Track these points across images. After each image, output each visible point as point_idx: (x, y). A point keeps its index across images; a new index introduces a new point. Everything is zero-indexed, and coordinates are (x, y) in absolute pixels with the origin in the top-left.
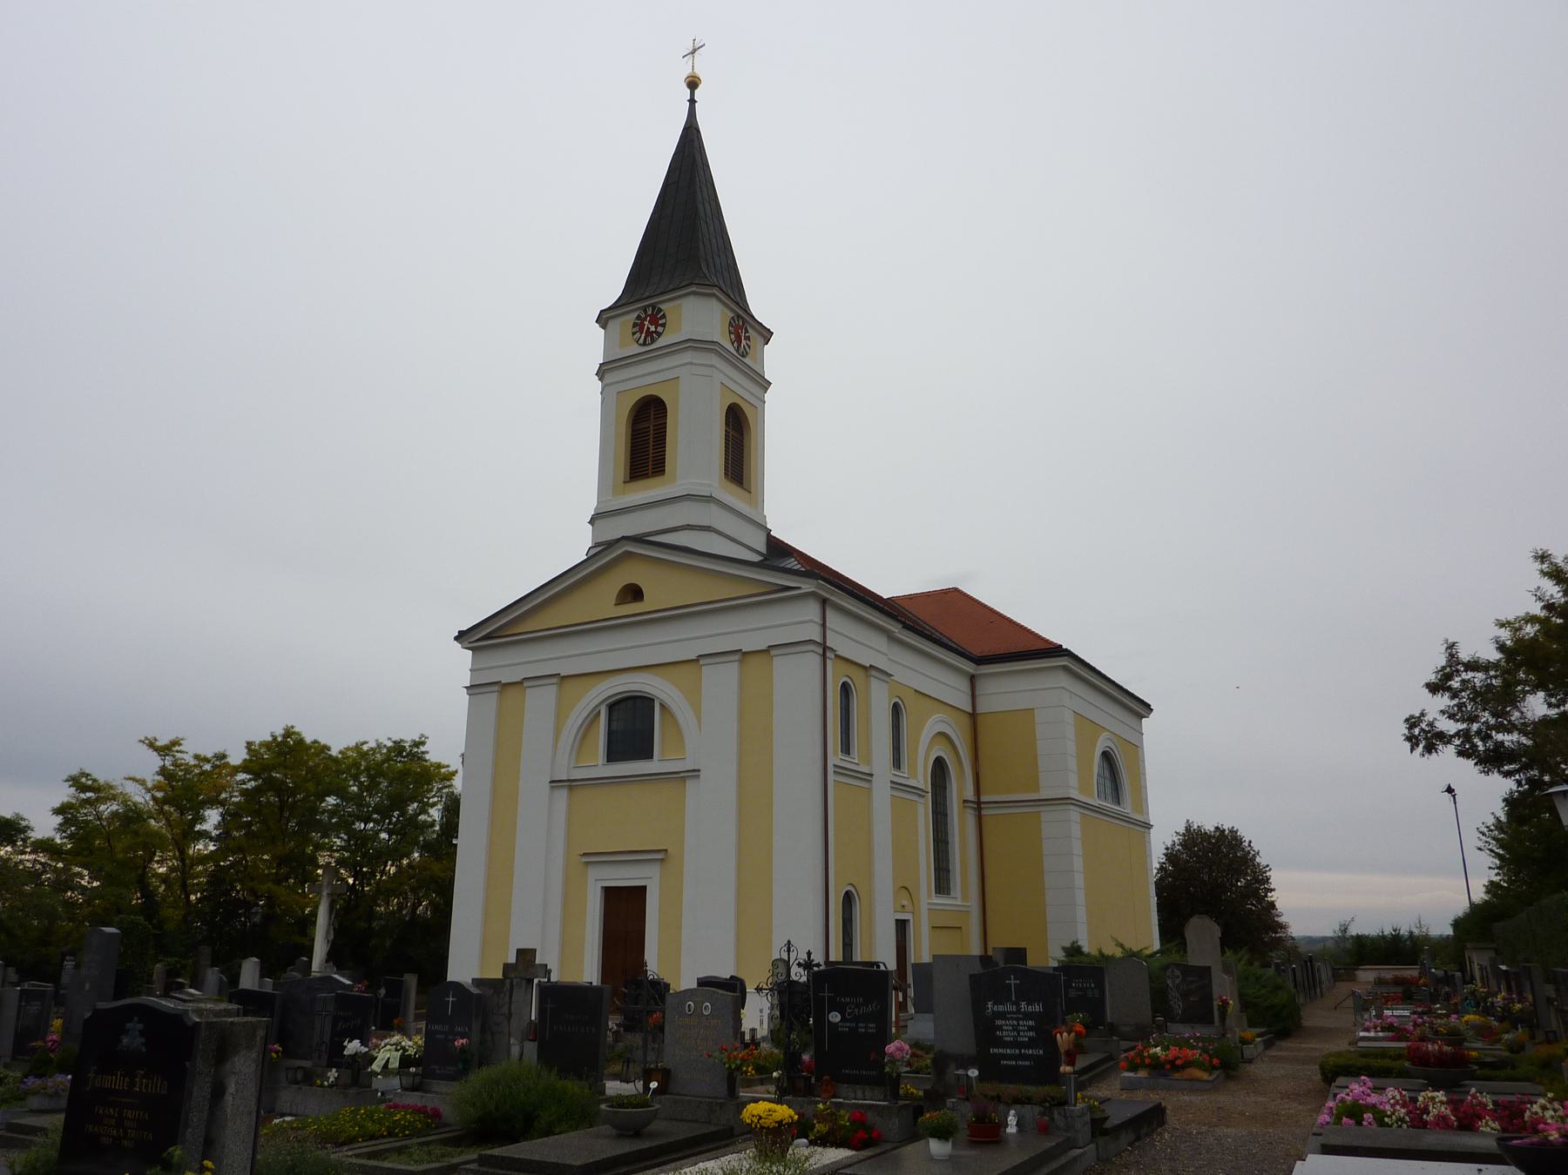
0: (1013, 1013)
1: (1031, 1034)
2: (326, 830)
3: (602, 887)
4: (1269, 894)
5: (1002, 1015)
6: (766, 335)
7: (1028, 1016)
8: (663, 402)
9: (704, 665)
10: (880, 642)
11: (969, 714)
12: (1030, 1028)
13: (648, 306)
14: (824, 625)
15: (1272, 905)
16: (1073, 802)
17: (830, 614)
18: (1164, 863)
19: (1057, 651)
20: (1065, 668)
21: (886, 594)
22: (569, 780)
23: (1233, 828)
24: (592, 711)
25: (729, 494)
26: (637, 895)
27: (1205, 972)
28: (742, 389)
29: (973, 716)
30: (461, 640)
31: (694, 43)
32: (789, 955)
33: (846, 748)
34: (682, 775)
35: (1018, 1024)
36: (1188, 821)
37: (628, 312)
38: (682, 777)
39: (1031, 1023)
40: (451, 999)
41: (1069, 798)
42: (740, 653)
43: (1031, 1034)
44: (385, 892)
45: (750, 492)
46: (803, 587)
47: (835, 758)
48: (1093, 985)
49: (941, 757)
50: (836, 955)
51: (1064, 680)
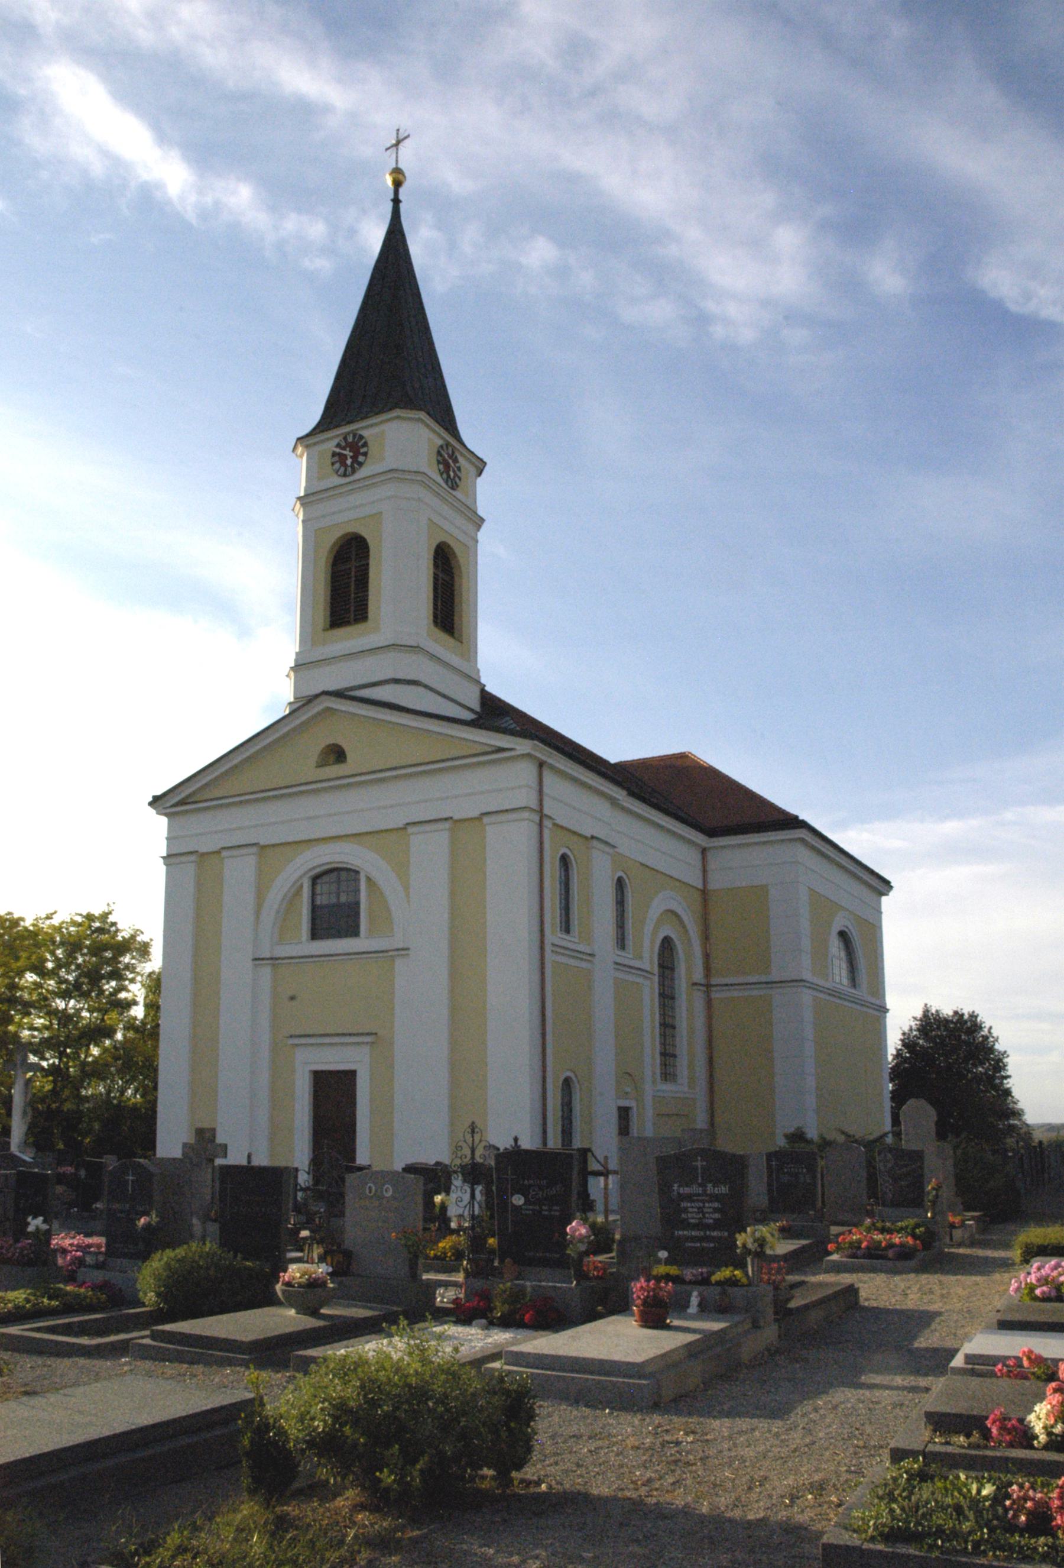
0: (699, 1195)
1: (717, 1216)
2: (26, 1008)
3: (310, 1071)
4: (1005, 1081)
5: (689, 1198)
6: (480, 466)
7: (714, 1198)
8: (367, 544)
9: (412, 834)
10: (602, 808)
11: (698, 889)
12: (716, 1210)
13: (349, 433)
14: (541, 792)
15: (1008, 1093)
16: (808, 985)
17: (548, 778)
18: (901, 1050)
19: (792, 822)
20: (802, 840)
21: (613, 759)
22: (272, 959)
23: (973, 1012)
24: (295, 882)
25: (438, 643)
26: (348, 1078)
27: (917, 1156)
28: (453, 529)
29: (704, 892)
30: (155, 805)
31: (398, 134)
32: (473, 1137)
33: (567, 929)
34: (391, 953)
35: (704, 1207)
36: (926, 1005)
37: (328, 439)
38: (391, 956)
39: (716, 1205)
40: (131, 1178)
41: (801, 981)
42: (450, 821)
43: (717, 1216)
44: (96, 1071)
45: (462, 642)
46: (517, 747)
47: (554, 936)
48: (805, 1170)
49: (670, 938)
50: (554, 1142)
51: (803, 854)
